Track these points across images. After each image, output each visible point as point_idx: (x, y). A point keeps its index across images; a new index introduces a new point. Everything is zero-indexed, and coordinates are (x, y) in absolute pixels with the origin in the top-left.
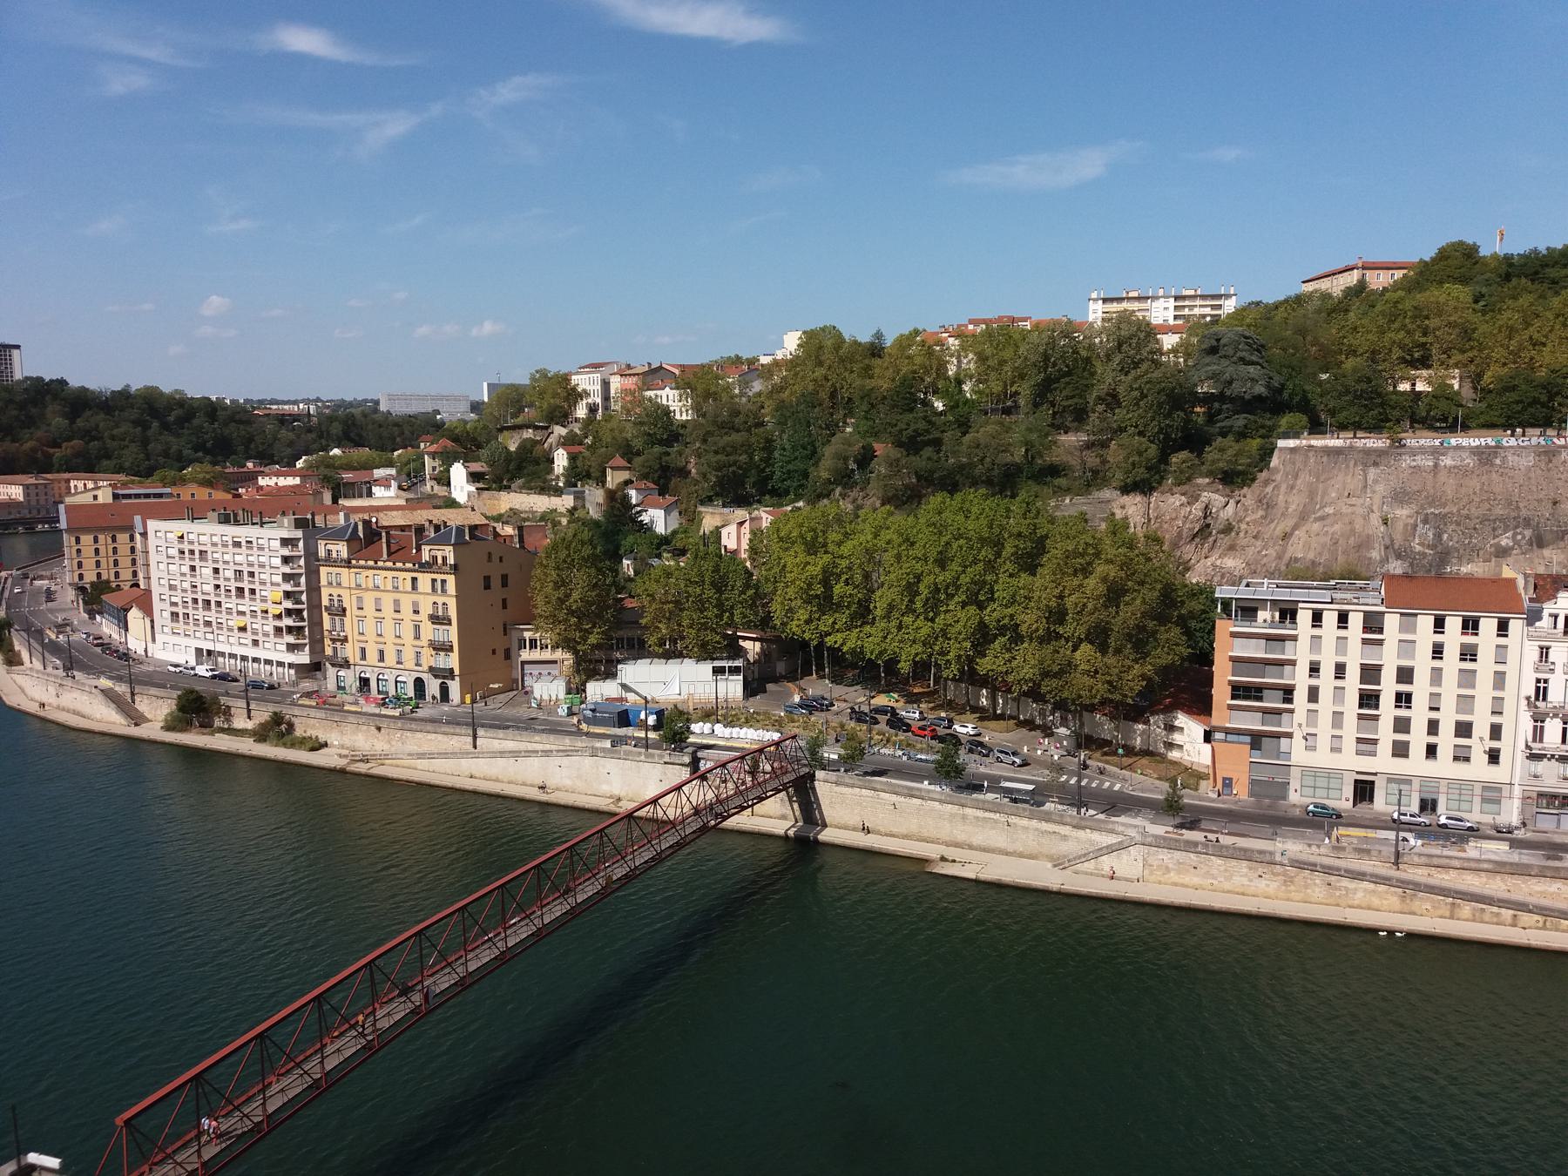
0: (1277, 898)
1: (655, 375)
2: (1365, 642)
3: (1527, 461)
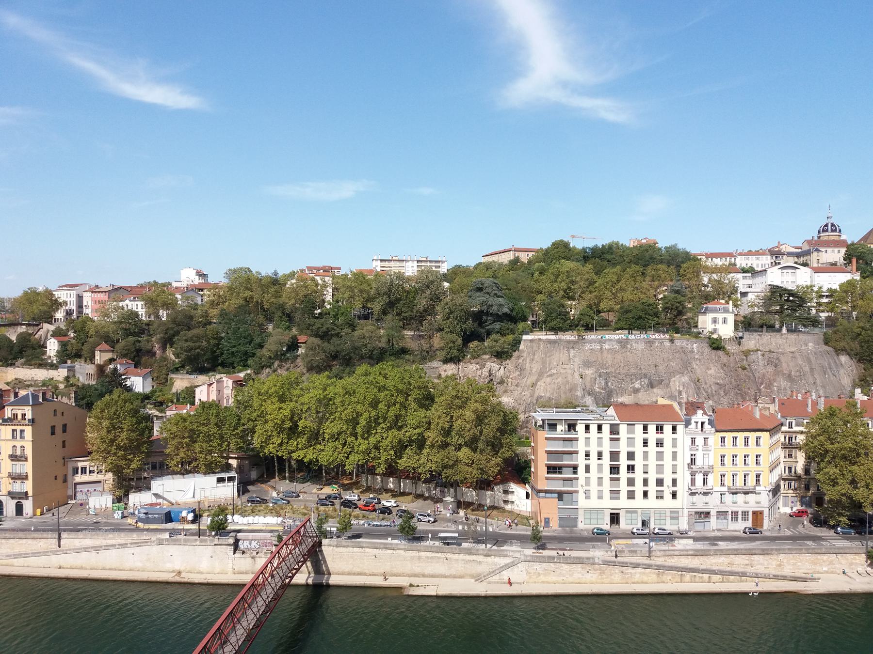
0: (597, 583)
1: (118, 292)
2: (611, 439)
3: (641, 346)
